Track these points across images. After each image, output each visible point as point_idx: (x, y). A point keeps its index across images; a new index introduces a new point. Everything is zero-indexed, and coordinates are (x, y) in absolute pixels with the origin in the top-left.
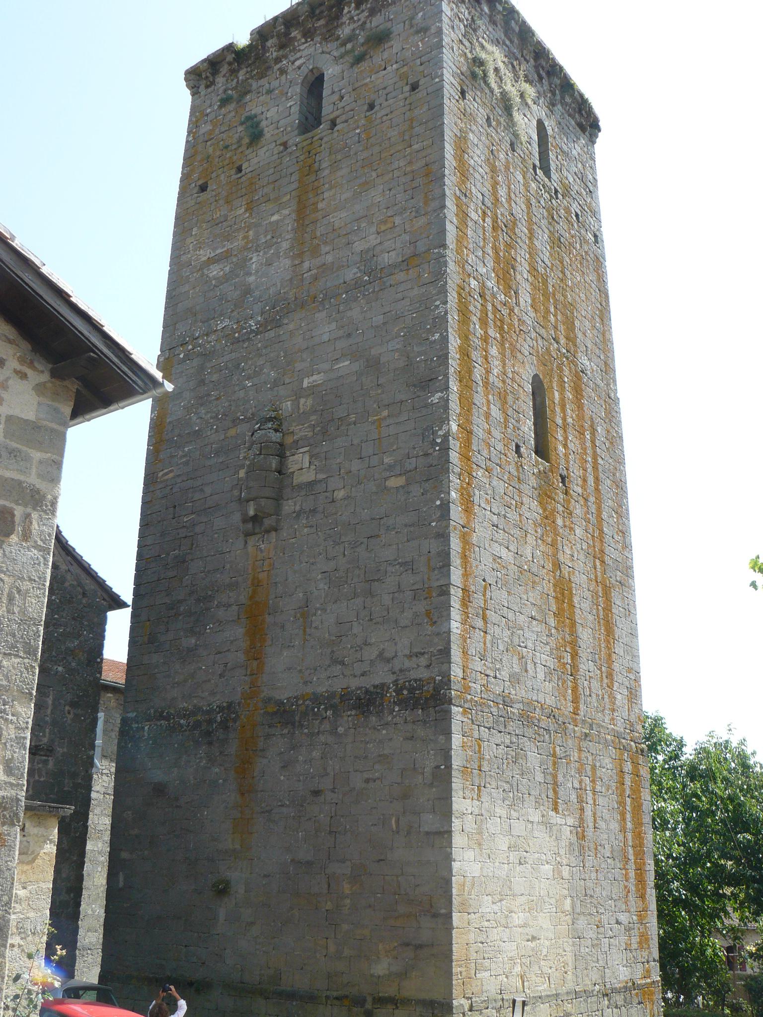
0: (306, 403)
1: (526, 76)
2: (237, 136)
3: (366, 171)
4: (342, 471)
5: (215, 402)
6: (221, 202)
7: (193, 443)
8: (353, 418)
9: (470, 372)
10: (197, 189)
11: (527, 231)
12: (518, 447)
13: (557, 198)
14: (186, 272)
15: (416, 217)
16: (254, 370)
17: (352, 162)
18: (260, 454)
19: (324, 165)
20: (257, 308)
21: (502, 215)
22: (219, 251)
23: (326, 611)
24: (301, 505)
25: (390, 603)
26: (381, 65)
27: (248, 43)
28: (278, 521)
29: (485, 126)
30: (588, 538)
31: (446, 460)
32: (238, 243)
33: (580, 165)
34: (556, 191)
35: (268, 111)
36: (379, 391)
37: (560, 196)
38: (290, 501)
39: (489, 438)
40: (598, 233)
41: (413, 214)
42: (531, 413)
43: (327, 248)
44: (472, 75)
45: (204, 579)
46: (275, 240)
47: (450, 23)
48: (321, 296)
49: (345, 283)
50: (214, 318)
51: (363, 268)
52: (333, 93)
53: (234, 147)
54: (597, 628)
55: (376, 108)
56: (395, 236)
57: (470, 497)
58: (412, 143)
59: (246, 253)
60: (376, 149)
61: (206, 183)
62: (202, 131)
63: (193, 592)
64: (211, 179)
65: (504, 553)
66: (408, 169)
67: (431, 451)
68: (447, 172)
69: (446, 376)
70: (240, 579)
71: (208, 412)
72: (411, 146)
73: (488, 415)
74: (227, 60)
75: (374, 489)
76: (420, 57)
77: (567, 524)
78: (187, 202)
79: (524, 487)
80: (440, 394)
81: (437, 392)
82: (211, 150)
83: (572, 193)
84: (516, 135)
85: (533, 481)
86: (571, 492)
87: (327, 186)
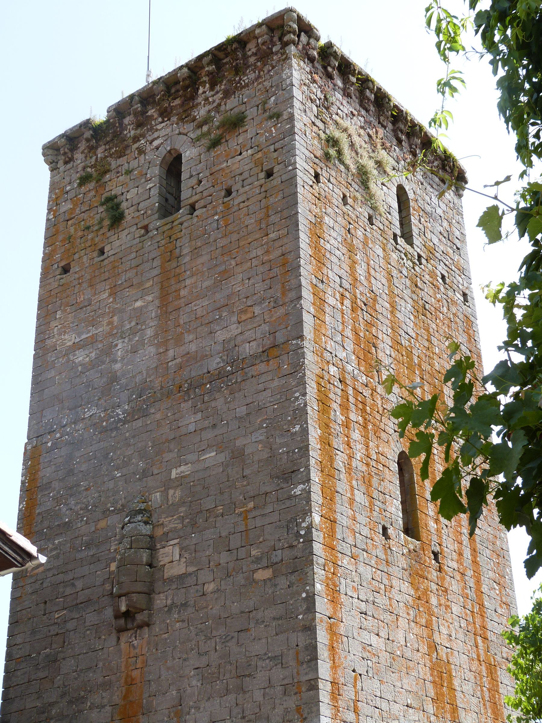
0: (175, 495)
1: (383, 144)
2: (98, 217)
3: (226, 259)
4: (212, 564)
5: (85, 493)
6: (85, 285)
7: (64, 535)
8: (220, 509)
9: (331, 460)
10: (59, 271)
11: (388, 305)
12: (385, 529)
13: (421, 264)
14: (51, 357)
15: (274, 308)
16: (123, 460)
17: (212, 249)
18: (131, 548)
19: (185, 251)
20: (124, 396)
21: (361, 293)
22: (84, 336)
23: (199, 709)
24: (173, 599)
25: (262, 699)
26: (236, 150)
27: (105, 119)
28: (150, 615)
29: (341, 206)
30: (466, 615)
31: (310, 552)
32: (103, 329)
33: (445, 224)
34: (420, 256)
35: (128, 192)
36: (245, 483)
37: (424, 261)
38: (161, 595)
39: (354, 524)
40: (467, 292)
41: (272, 304)
42: (398, 492)
43: (191, 337)
44: (326, 156)
45: (76, 679)
46: (139, 327)
47: (302, 107)
48: (186, 385)
49: (209, 372)
50: (81, 405)
51: (225, 358)
52: (191, 176)
53: (96, 228)
54: (482, 712)
55: (234, 194)
56: (255, 325)
57: (336, 586)
58: (269, 232)
59: (111, 340)
60: (235, 237)
61: (69, 264)
62: (63, 210)
63: (65, 694)
64: (73, 260)
65: (374, 640)
66: (266, 258)
67: (295, 543)
68: (302, 262)
69: (307, 467)
70: (113, 678)
71: (77, 503)
72: (267, 235)
73: (352, 501)
74: (85, 136)
75: (243, 582)
76: (274, 144)
77: (443, 601)
78: (49, 284)
79: (392, 570)
80: (302, 486)
81: (300, 483)
82: (72, 230)
83: (437, 255)
84: (374, 208)
85: (403, 562)
86: (446, 568)
87: (188, 273)
